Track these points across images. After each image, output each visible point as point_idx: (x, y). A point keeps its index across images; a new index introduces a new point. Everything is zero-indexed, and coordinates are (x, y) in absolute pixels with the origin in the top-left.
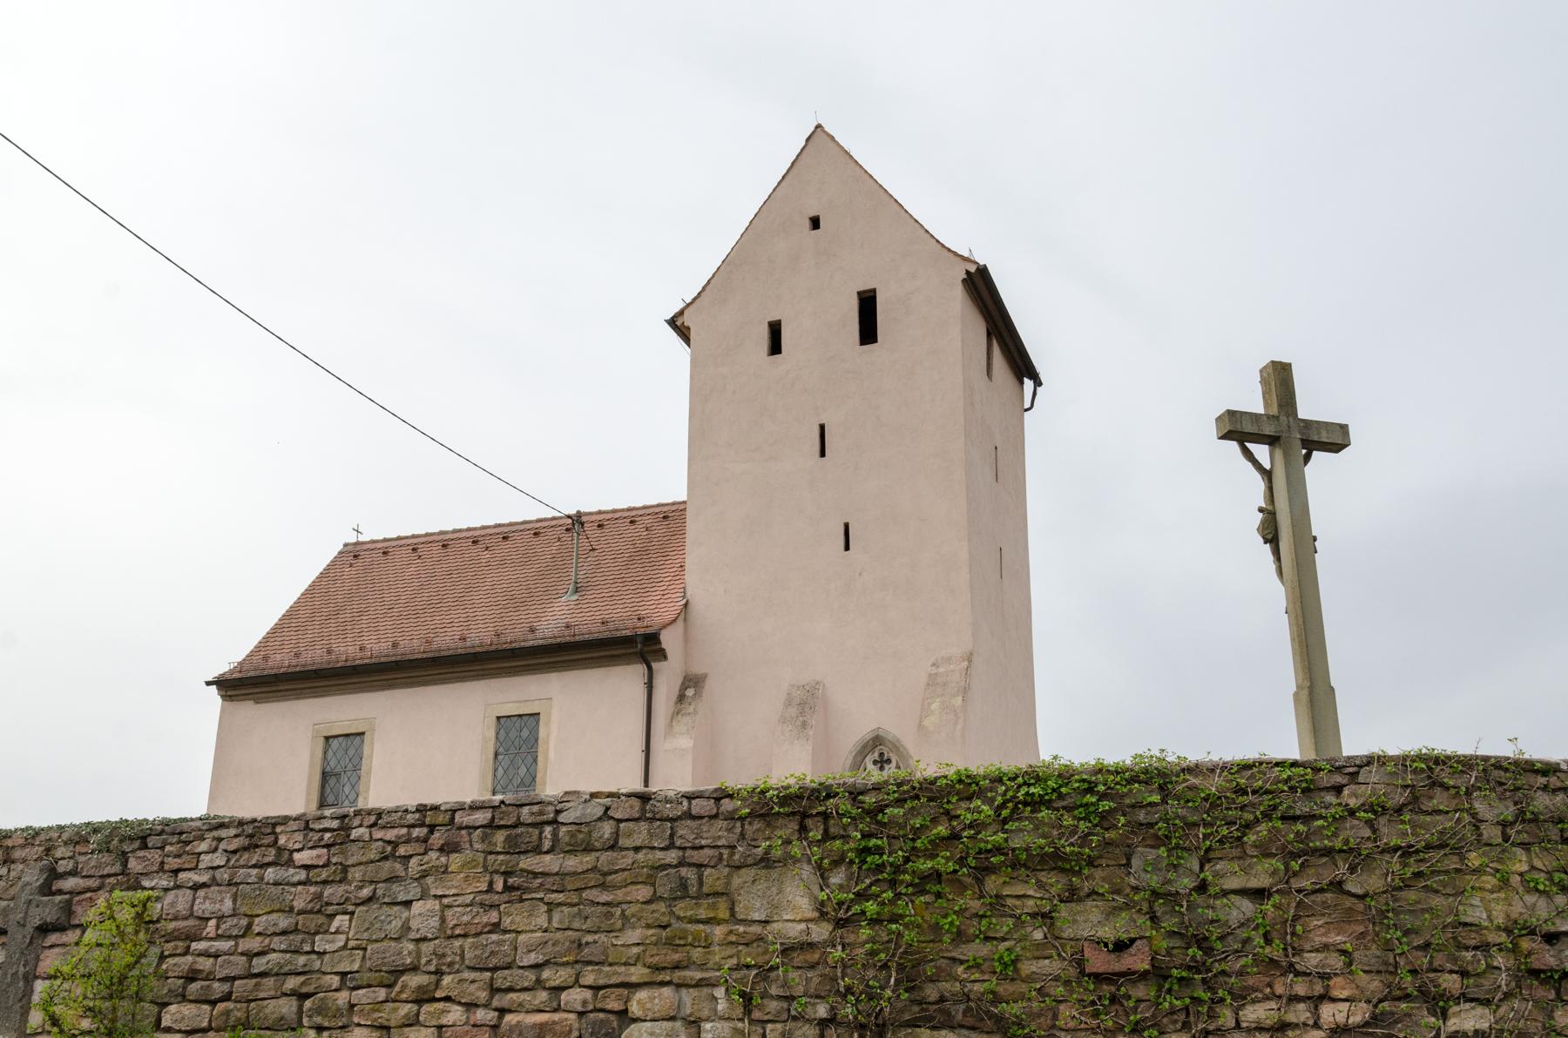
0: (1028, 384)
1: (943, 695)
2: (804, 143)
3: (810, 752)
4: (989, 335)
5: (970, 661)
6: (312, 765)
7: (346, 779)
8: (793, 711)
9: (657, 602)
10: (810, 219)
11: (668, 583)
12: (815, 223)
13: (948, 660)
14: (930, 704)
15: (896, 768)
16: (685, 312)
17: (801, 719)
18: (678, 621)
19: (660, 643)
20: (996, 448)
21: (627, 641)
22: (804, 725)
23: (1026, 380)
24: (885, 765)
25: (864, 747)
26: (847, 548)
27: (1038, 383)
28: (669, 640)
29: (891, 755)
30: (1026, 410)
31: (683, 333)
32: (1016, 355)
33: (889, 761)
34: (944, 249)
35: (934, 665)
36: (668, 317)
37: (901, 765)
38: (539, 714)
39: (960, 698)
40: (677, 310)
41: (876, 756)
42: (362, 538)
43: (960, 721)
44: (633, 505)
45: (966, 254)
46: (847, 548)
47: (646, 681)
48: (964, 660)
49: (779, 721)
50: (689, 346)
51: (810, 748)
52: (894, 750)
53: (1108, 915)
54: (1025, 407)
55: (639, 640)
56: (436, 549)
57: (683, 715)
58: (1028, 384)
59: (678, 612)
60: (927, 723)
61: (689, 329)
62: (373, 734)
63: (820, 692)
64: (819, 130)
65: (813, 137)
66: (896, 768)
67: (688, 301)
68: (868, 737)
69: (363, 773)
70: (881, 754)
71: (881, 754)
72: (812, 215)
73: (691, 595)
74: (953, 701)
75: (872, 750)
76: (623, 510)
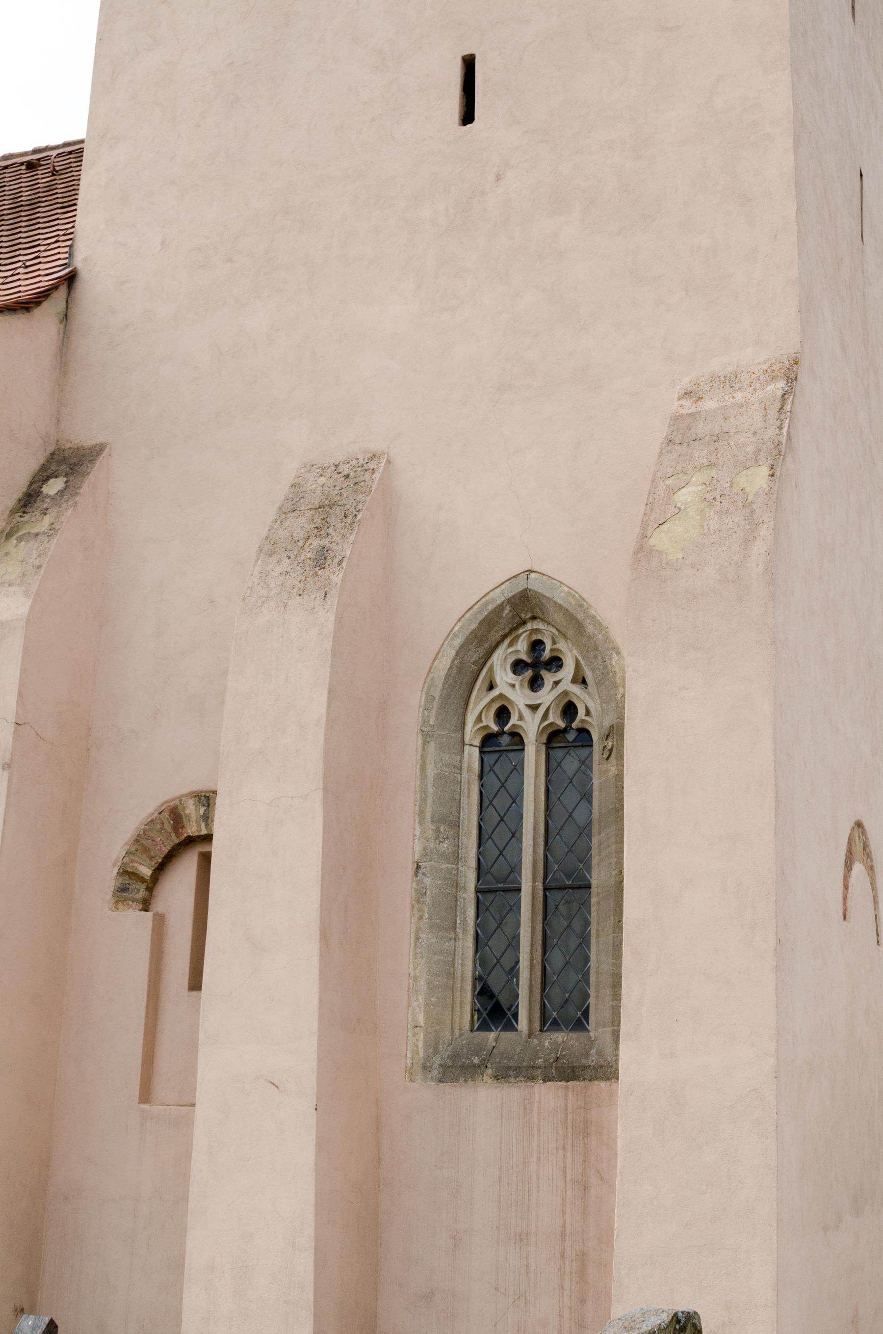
1: (712, 465)
3: (331, 625)
5: (791, 379)
8: (299, 525)
13: (730, 381)
14: (672, 491)
15: (574, 681)
17: (316, 543)
22: (322, 558)
24: (544, 673)
25: (489, 622)
26: (468, 117)
29: (562, 645)
33: (555, 663)
35: (687, 394)
39: (764, 471)
41: (522, 647)
43: (763, 531)
46: (468, 117)
48: (774, 379)
49: (260, 550)
51: (332, 617)
52: (570, 633)
53: (35, 536)
57: (20, 539)
60: (659, 540)
63: (377, 475)
66: (574, 681)
68: (499, 597)
70: (536, 646)
71: (536, 646)
73: (85, 260)
74: (742, 481)
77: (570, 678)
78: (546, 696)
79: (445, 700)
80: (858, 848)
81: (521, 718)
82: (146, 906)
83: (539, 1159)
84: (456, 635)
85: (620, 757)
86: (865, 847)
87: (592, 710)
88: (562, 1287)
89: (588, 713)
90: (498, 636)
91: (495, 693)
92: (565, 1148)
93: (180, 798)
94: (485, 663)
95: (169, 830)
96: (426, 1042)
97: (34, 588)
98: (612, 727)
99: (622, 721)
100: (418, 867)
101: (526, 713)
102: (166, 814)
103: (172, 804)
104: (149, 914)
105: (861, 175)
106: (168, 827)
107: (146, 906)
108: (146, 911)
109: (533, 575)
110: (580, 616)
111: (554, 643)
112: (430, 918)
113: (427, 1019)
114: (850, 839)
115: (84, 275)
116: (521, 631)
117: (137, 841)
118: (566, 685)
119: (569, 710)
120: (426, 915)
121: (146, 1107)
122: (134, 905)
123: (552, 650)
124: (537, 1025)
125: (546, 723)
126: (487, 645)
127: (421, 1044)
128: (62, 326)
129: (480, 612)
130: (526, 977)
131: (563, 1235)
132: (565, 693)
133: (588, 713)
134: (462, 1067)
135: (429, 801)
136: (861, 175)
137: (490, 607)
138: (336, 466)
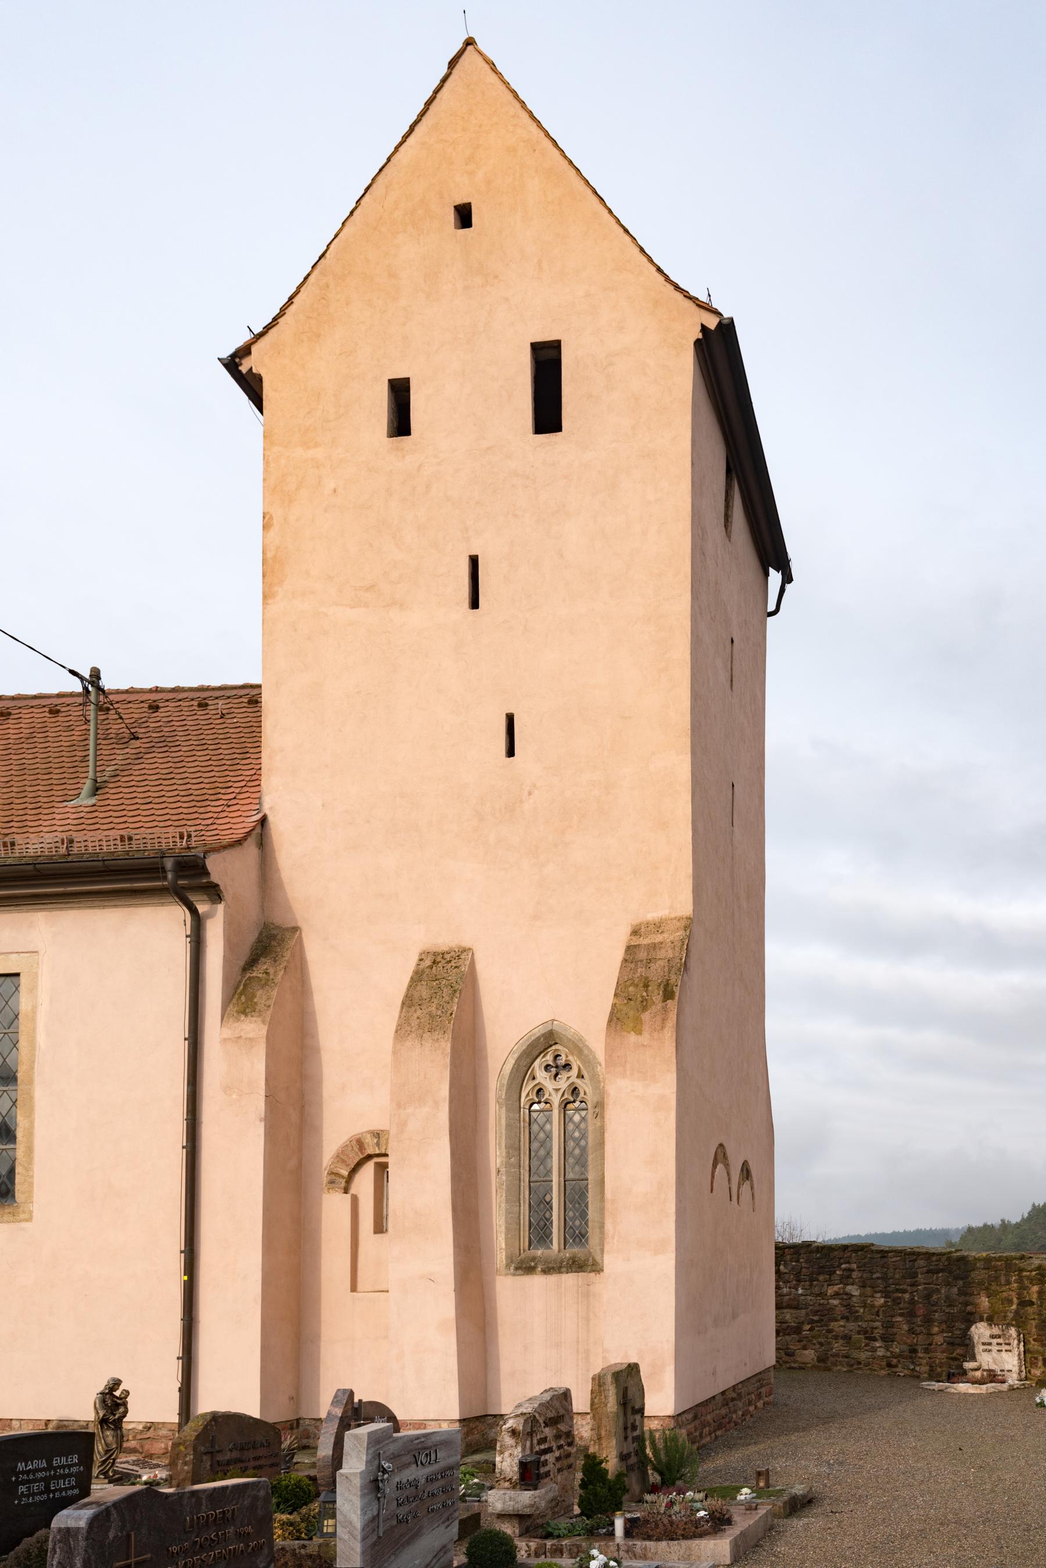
3: (449, 1050)
4: (729, 471)
9: (215, 815)
10: (455, 207)
11: (237, 791)
12: (464, 216)
16: (254, 349)
18: (246, 844)
20: (732, 641)
23: (772, 571)
25: (532, 1045)
26: (511, 752)
27: (788, 578)
29: (570, 1058)
30: (771, 614)
33: (567, 1066)
34: (668, 285)
36: (226, 353)
38: (18, 975)
41: (549, 1058)
44: (206, 684)
45: (703, 298)
46: (511, 752)
47: (189, 933)
54: (769, 611)
55: (169, 864)
58: (775, 577)
59: (247, 830)
64: (470, 48)
65: (461, 60)
66: (578, 1077)
67: (257, 330)
68: (538, 1032)
72: (460, 200)
73: (271, 808)
75: (544, 1051)
76: (191, 690)
77: (576, 1076)
78: (563, 1083)
80: (720, 1156)
81: (550, 1095)
83: (565, 1309)
84: (515, 1053)
85: (603, 1118)
86: (725, 1154)
87: (587, 1092)
88: (578, 1365)
89: (585, 1094)
90: (537, 1053)
91: (536, 1082)
92: (578, 1303)
93: (362, 1133)
94: (530, 1066)
95: (357, 1150)
96: (506, 1256)
97: (268, 1019)
98: (598, 1102)
99: (609, 1379)
100: (499, 1171)
101: (553, 1093)
102: (355, 1142)
103: (358, 1137)
104: (348, 1196)
105: (733, 786)
106: (356, 1149)
108: (346, 1193)
109: (555, 1022)
110: (581, 1045)
111: (567, 1057)
112: (506, 1196)
113: (506, 1245)
114: (716, 1152)
115: (271, 818)
116: (549, 1050)
117: (338, 1156)
118: (574, 1079)
119: (575, 1091)
120: (504, 1195)
121: (355, 1294)
122: (339, 1190)
123: (566, 1061)
124: (562, 1246)
125: (564, 1098)
126: (531, 1057)
127: (504, 1257)
128: (260, 851)
129: (527, 1040)
130: (502, 1162)
131: (578, 1342)
132: (573, 1083)
133: (585, 1094)
134: (525, 1268)
135: (504, 1138)
136: (733, 786)
137: (533, 1038)
138: (443, 954)
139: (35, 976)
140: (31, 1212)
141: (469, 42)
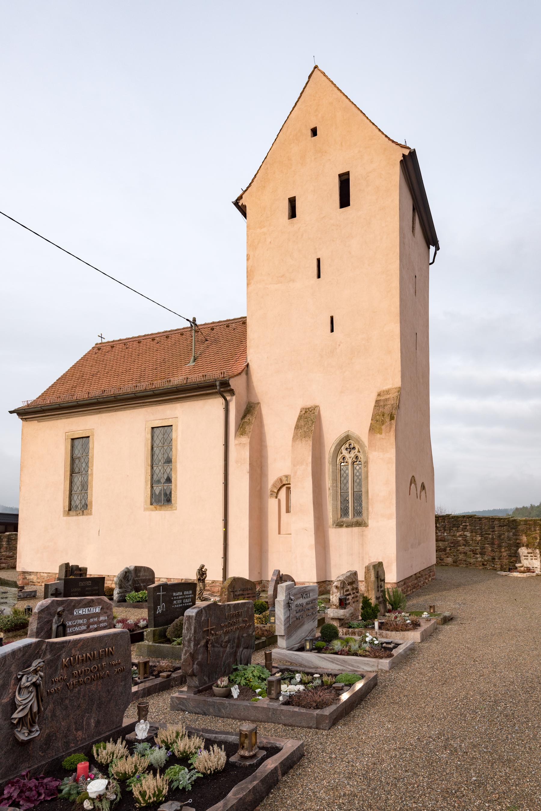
0: (432, 249)
2: (307, 80)
4: (414, 209)
6: (66, 453)
7: (83, 460)
12: (314, 132)
18: (242, 374)
19: (230, 386)
21: (211, 386)
25: (341, 441)
26: (332, 331)
27: (437, 248)
28: (234, 383)
30: (431, 264)
31: (243, 210)
32: (427, 227)
37: (361, 451)
38: (172, 426)
40: (238, 195)
41: (347, 445)
42: (104, 341)
45: (403, 143)
46: (332, 331)
50: (246, 218)
55: (218, 383)
56: (135, 344)
58: (432, 249)
61: (246, 207)
62: (93, 437)
67: (244, 189)
68: (343, 436)
69: (90, 457)
72: (312, 127)
73: (250, 360)
75: (345, 443)
79: (333, 456)
80: (413, 481)
82: (276, 497)
85: (367, 467)
91: (342, 455)
97: (250, 436)
101: (349, 458)
104: (277, 499)
107: (276, 497)
118: (356, 453)
119: (357, 457)
131: (359, 553)
139: (177, 426)
140: (176, 507)
141: (316, 67)
